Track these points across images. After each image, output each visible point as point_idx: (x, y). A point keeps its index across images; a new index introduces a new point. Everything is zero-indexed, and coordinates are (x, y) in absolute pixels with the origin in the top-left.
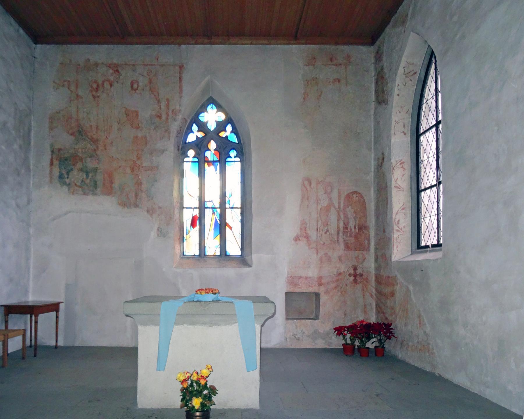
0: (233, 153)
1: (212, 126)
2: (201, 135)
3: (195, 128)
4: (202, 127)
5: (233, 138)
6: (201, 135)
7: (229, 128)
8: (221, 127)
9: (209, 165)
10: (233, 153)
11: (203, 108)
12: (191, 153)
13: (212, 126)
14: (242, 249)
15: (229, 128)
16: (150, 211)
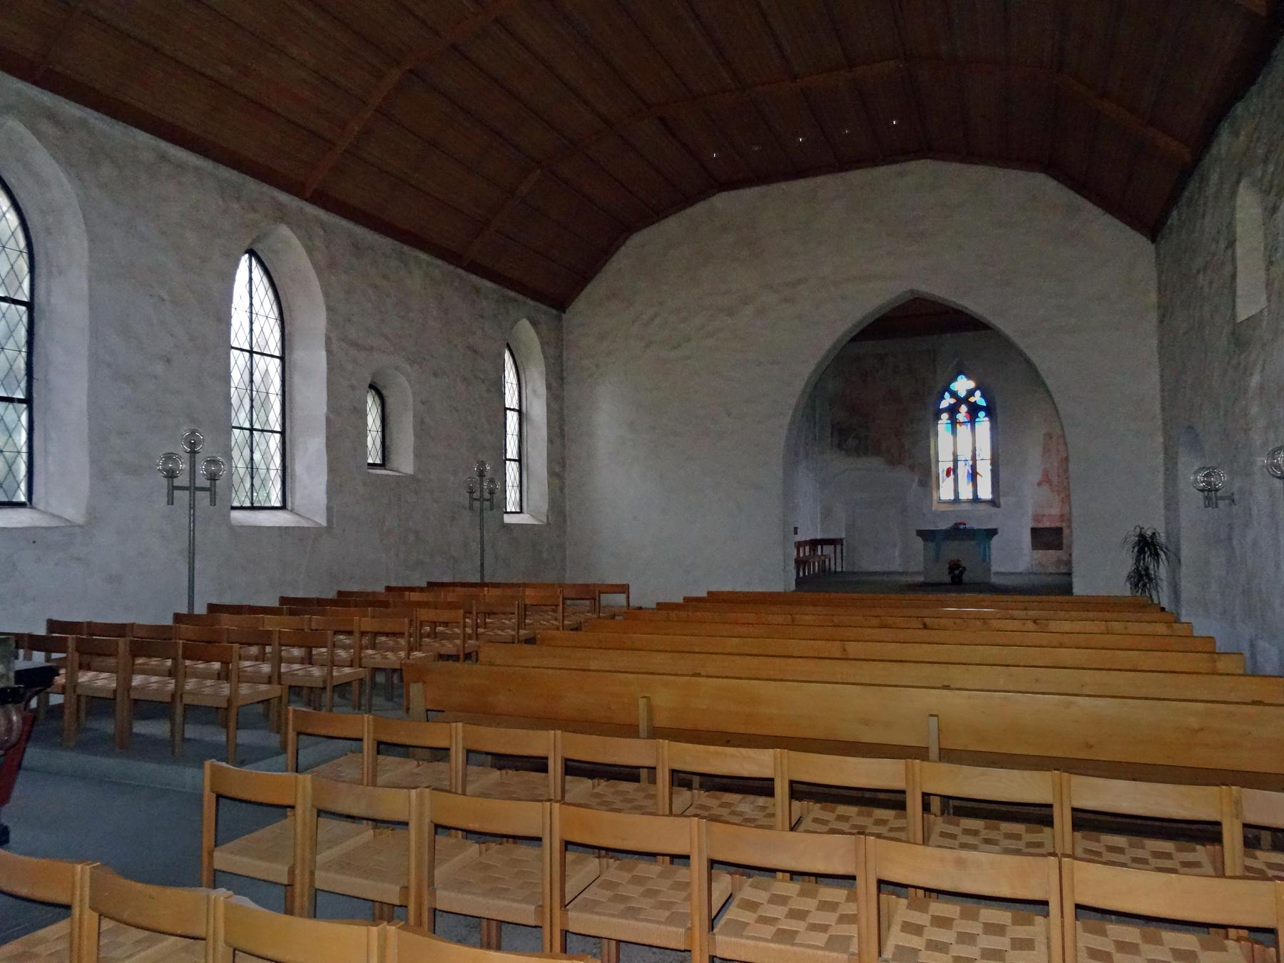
0: (982, 414)
1: (962, 394)
2: (953, 401)
3: (947, 395)
4: (954, 394)
5: (982, 402)
6: (953, 401)
7: (978, 393)
8: (971, 393)
9: (961, 426)
10: (982, 414)
11: (954, 379)
12: (945, 416)
13: (962, 394)
14: (993, 492)
15: (978, 393)
16: (912, 468)
